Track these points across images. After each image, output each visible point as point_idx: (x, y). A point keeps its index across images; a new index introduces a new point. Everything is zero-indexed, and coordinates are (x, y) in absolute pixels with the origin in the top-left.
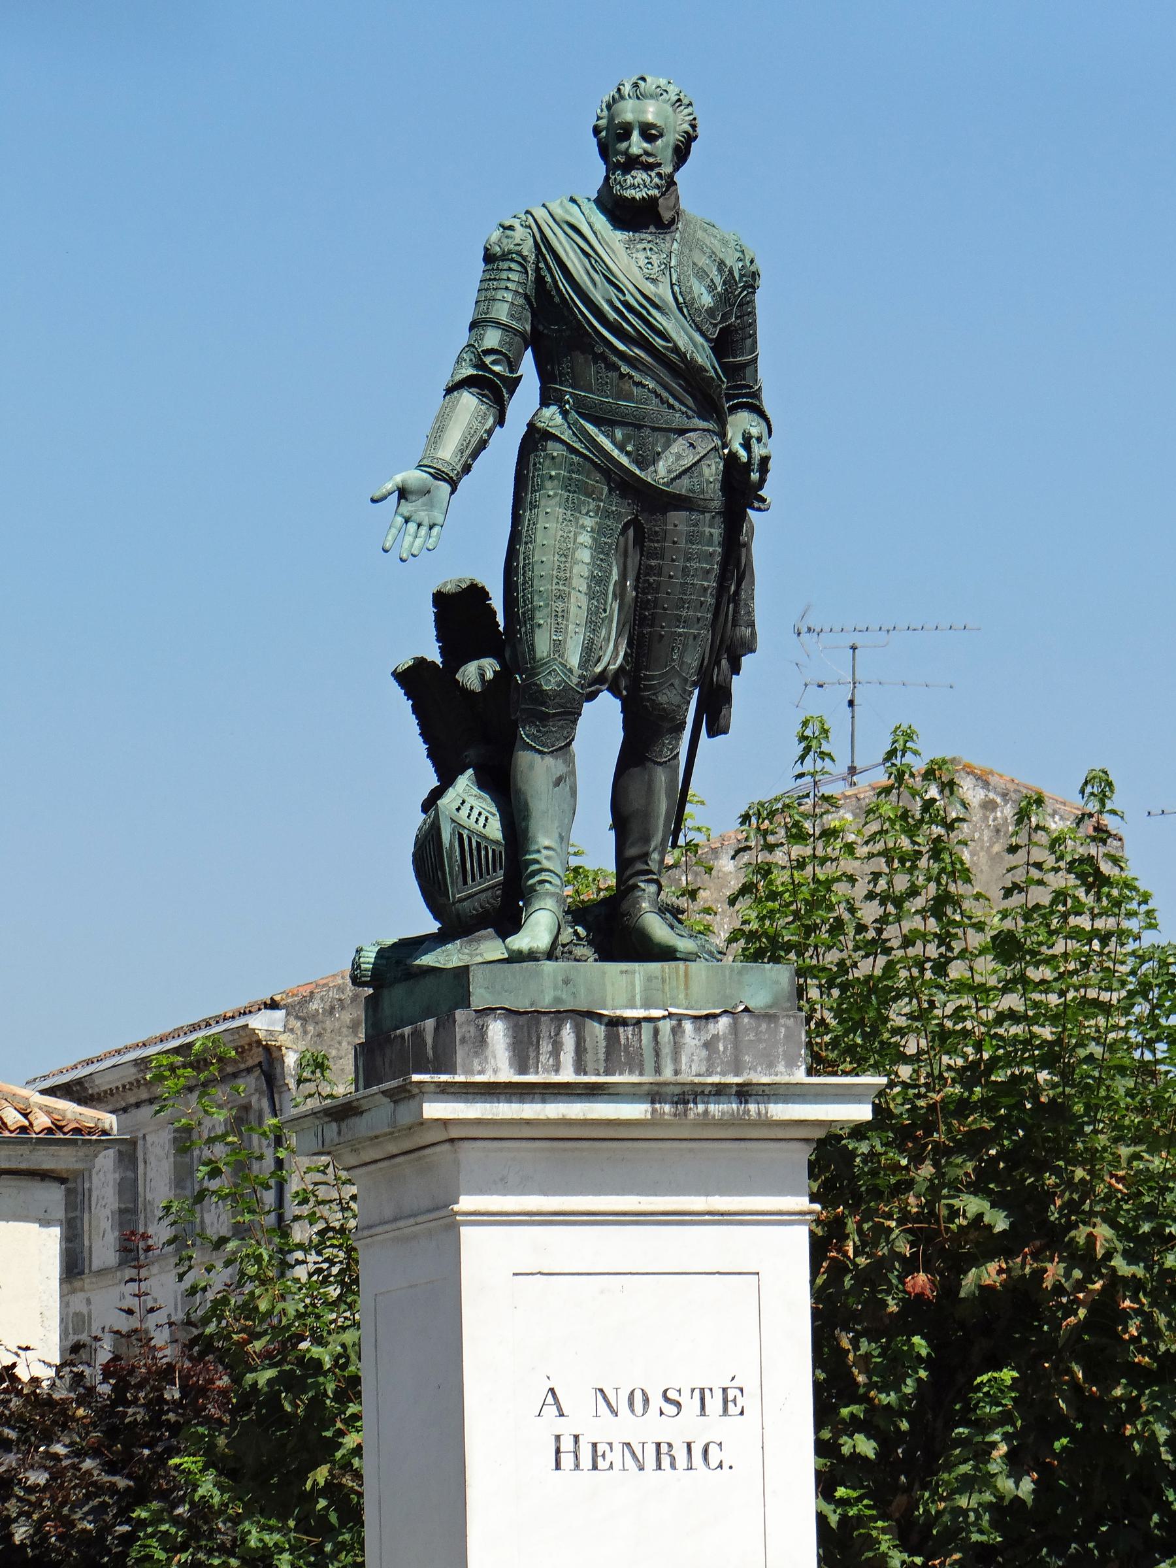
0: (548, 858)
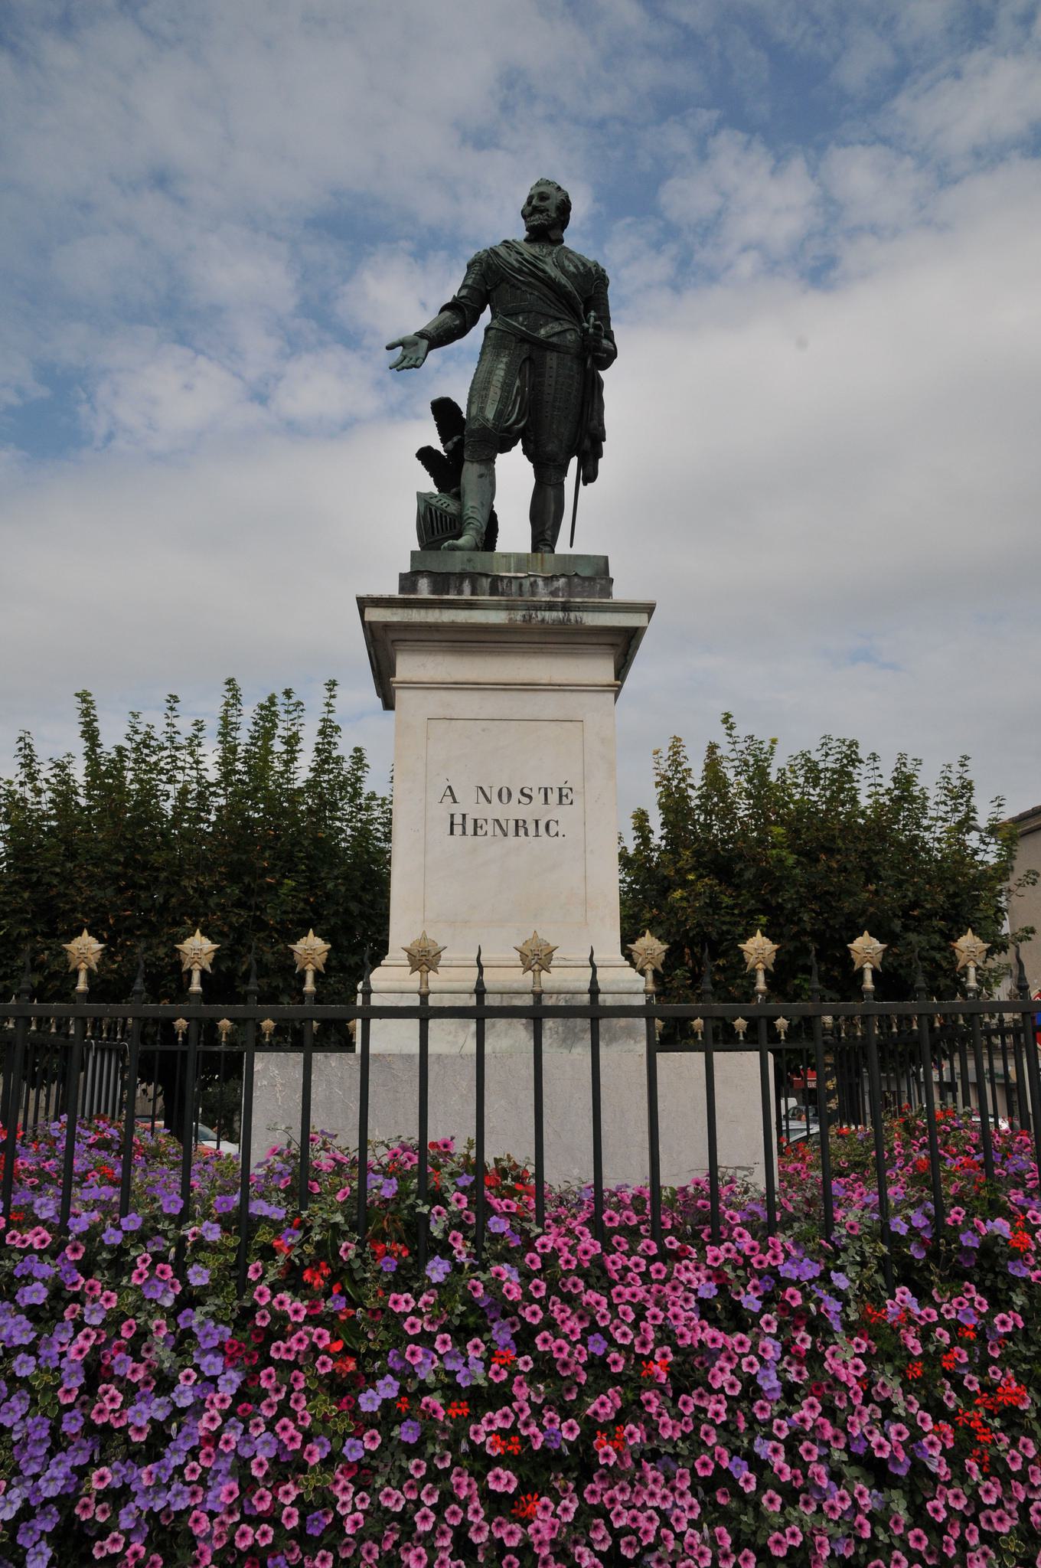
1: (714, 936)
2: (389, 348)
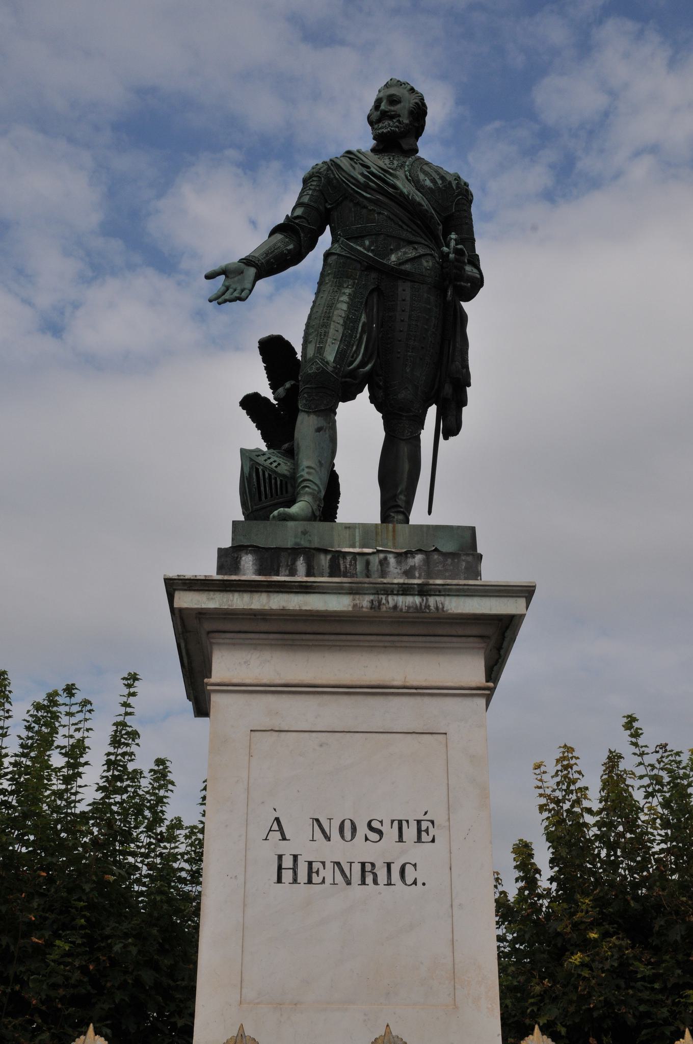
0: (308, 473)
1: (631, 1020)
2: (209, 277)
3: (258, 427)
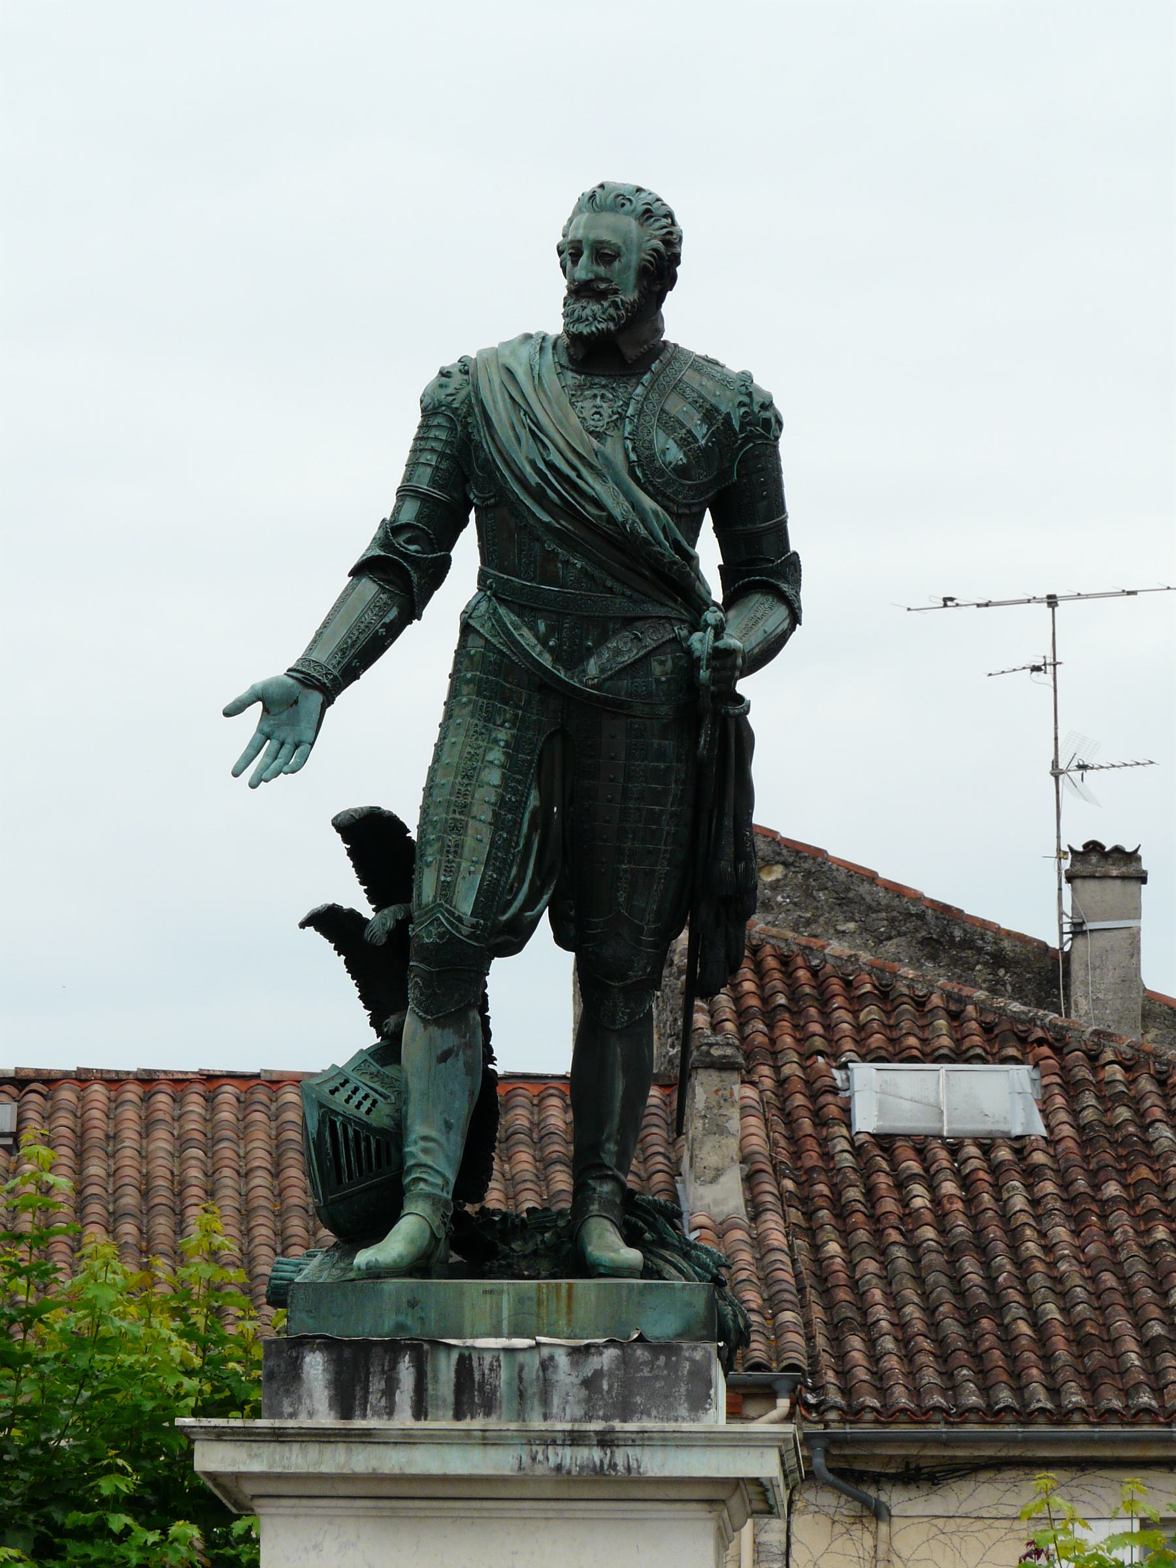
0: (425, 1151)
2: (232, 711)
3: (340, 949)
